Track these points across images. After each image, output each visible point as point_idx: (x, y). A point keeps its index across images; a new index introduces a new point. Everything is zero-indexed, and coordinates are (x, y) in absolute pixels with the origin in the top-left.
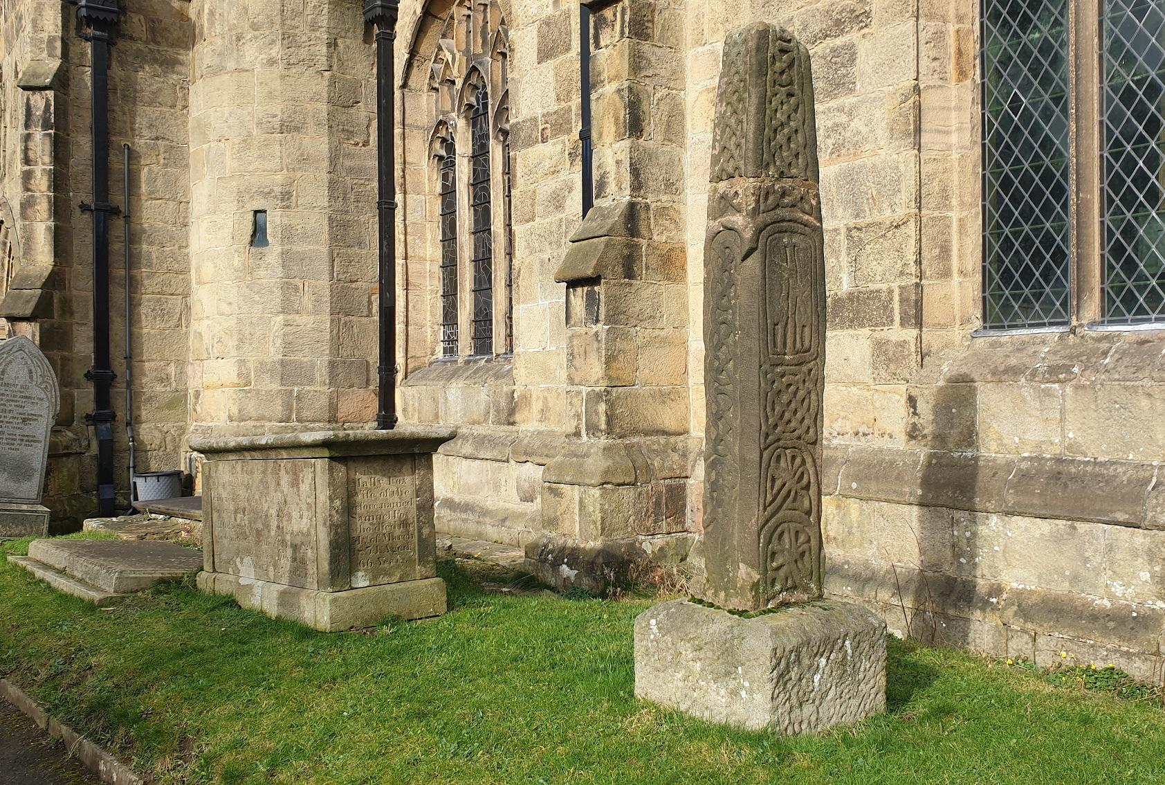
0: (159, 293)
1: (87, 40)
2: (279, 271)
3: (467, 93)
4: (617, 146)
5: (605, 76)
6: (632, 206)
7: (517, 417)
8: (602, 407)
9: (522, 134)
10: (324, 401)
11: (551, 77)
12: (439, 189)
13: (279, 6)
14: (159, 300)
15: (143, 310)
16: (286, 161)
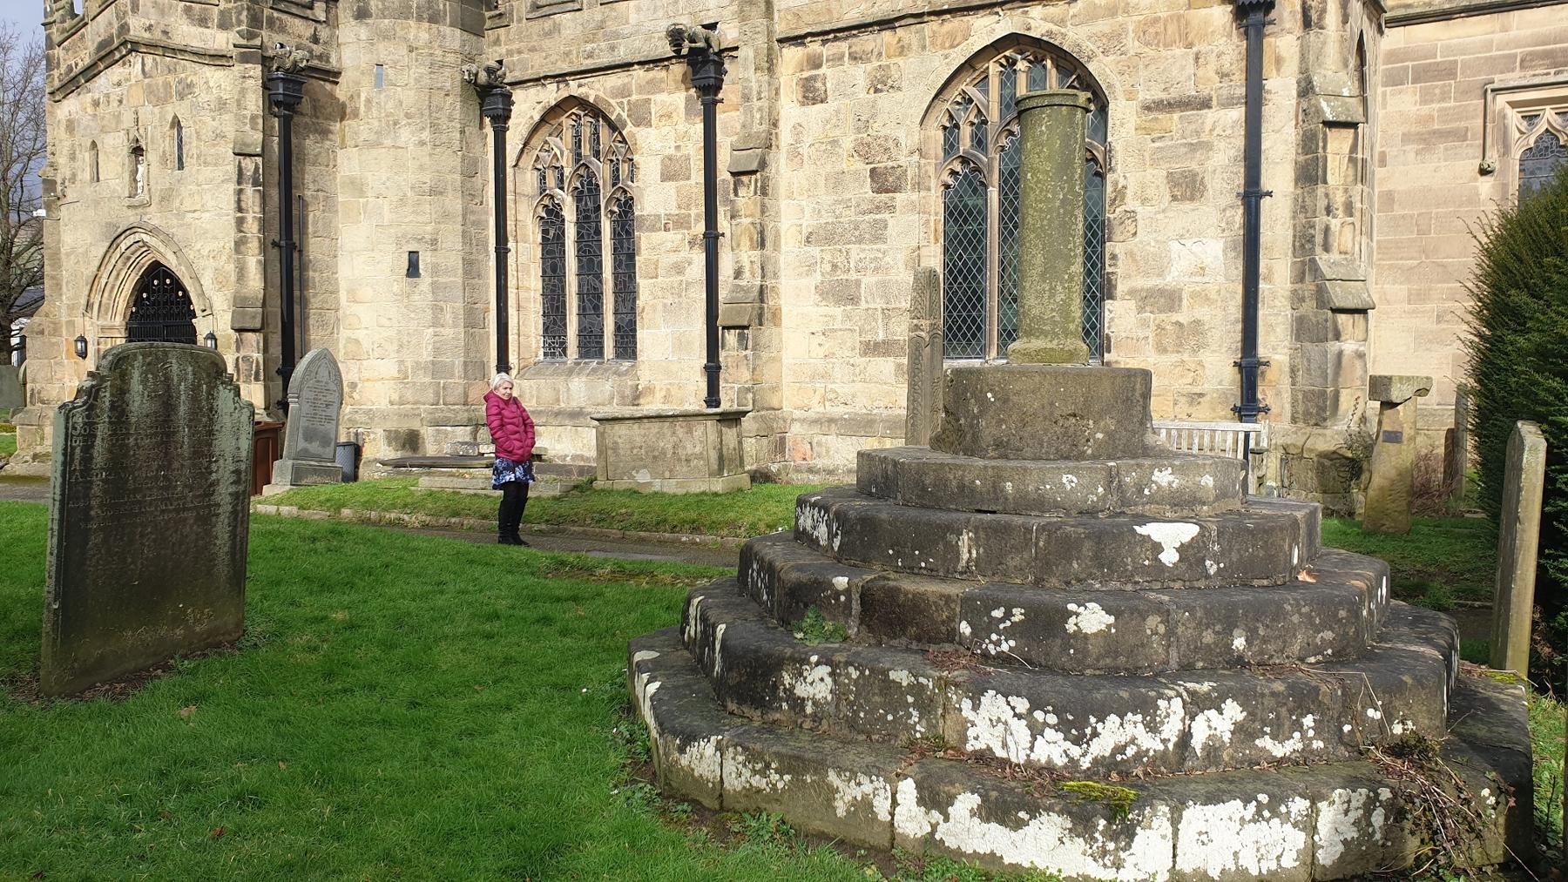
0: (320, 309)
1: (275, 116)
2: (430, 297)
3: (574, 180)
4: (750, 253)
5: (742, 213)
6: (762, 286)
7: (642, 401)
8: (750, 396)
9: (647, 224)
10: (461, 390)
11: (673, 192)
12: (539, 240)
13: (427, 103)
14: (320, 314)
15: (311, 321)
16: (434, 216)
